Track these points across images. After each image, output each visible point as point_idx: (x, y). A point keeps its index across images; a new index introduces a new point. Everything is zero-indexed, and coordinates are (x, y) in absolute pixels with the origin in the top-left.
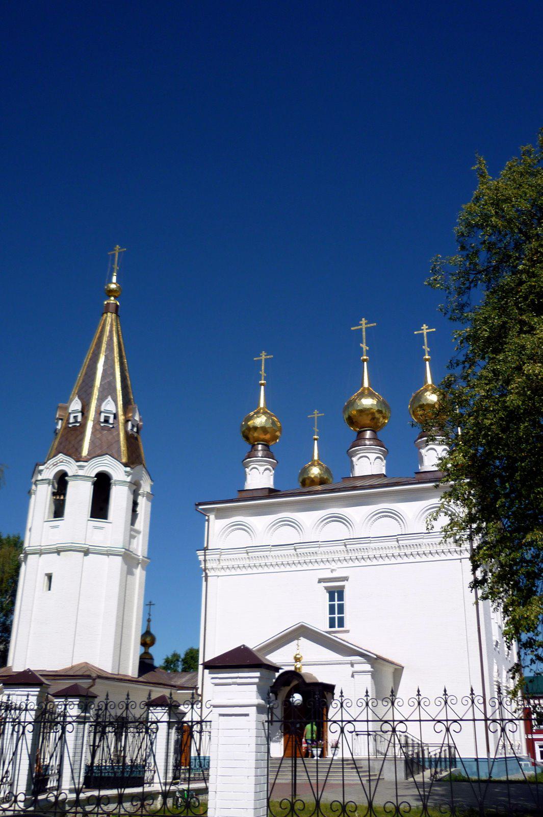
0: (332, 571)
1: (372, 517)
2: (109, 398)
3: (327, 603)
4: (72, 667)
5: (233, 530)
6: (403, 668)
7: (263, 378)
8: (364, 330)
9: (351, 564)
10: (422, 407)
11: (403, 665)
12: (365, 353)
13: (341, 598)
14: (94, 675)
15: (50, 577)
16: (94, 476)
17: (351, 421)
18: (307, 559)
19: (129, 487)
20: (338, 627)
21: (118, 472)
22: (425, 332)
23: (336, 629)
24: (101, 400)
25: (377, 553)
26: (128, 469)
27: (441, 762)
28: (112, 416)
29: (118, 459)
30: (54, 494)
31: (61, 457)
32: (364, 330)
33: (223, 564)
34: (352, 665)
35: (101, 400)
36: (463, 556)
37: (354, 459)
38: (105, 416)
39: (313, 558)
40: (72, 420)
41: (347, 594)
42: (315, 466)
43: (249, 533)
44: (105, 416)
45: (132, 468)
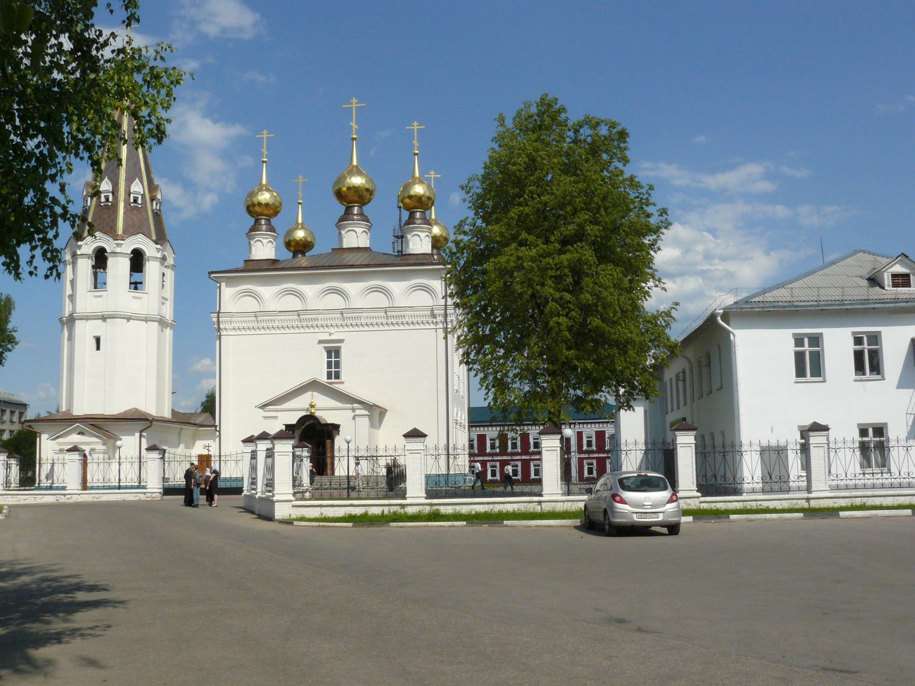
0: (330, 334)
1: (365, 291)
2: (137, 180)
3: (325, 360)
4: (126, 412)
5: (242, 297)
6: (387, 410)
7: (265, 156)
8: (354, 109)
9: (346, 329)
10: (410, 197)
11: (387, 408)
12: (354, 132)
14: (150, 419)
15: (98, 340)
16: (130, 253)
17: (339, 195)
18: (310, 324)
21: (150, 249)
22: (416, 128)
23: (333, 380)
24: (129, 181)
25: (369, 321)
26: (159, 246)
28: (140, 197)
29: (149, 237)
30: (93, 267)
32: (354, 109)
33: (236, 325)
34: (354, 410)
35: (129, 181)
36: (438, 327)
37: (343, 232)
38: (134, 197)
39: (314, 323)
40: (103, 199)
42: (301, 229)
43: (259, 303)
44: (134, 197)
45: (161, 245)
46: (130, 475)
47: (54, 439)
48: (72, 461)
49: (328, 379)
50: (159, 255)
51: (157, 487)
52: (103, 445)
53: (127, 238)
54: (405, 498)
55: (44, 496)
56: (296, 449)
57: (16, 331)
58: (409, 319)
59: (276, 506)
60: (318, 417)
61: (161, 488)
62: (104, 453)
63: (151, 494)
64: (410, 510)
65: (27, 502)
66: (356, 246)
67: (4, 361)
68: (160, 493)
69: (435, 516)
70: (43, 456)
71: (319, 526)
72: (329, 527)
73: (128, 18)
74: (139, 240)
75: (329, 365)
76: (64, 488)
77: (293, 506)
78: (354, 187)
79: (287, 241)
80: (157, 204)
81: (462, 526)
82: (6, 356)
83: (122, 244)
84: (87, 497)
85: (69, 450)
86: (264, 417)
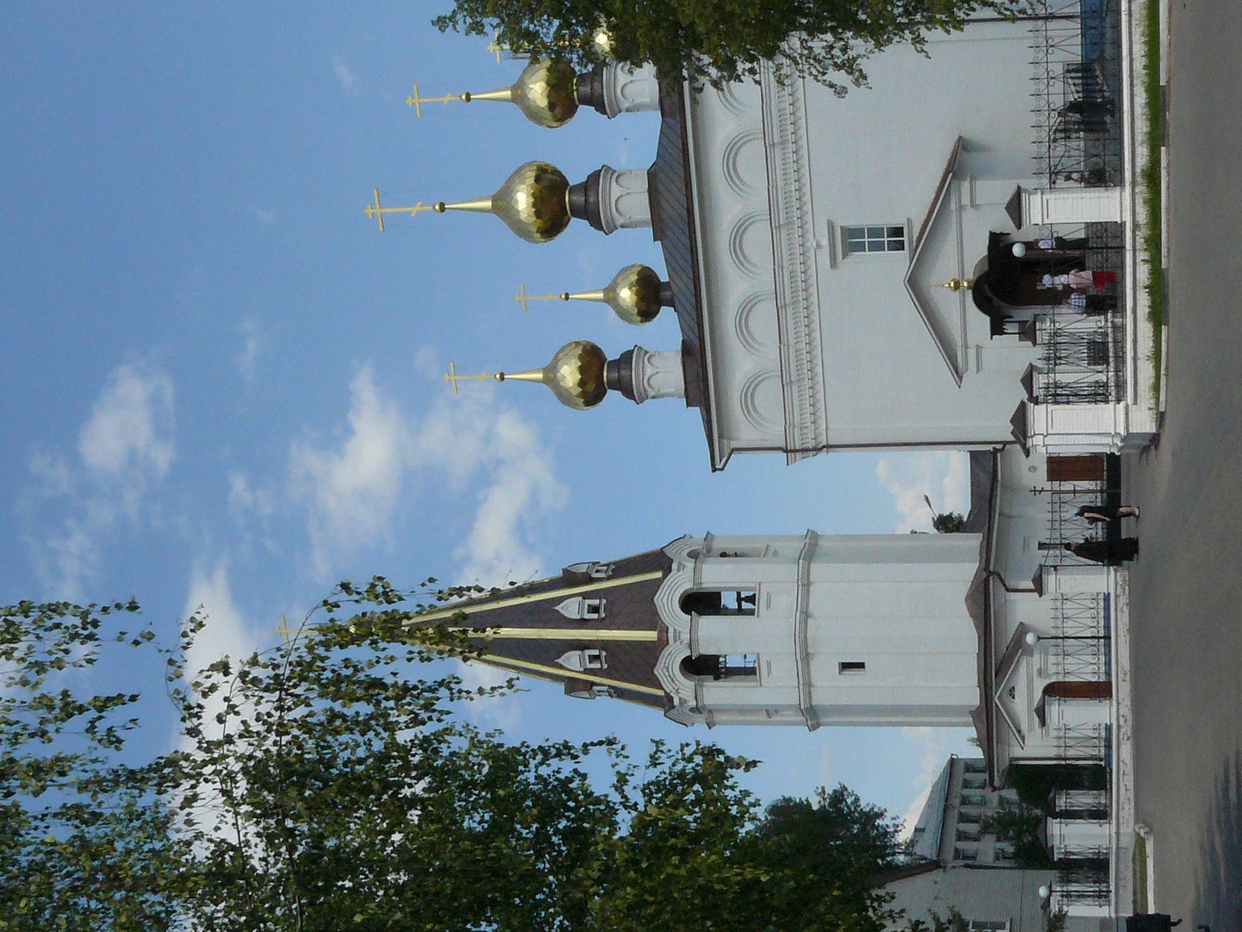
0: (819, 246)
2: (558, 608)
4: (972, 615)
5: (755, 409)
9: (808, 218)
13: (858, 232)
14: (984, 575)
15: (846, 666)
19: (702, 563)
20: (903, 236)
21: (680, 582)
22: (416, 101)
23: (905, 239)
26: (674, 566)
27: (1087, 84)
29: (657, 584)
30: (717, 678)
31: (660, 671)
33: (808, 419)
38: (588, 613)
40: (596, 665)
41: (852, 222)
46: (1084, 602)
47: (1023, 739)
48: (1061, 715)
49: (903, 249)
50: (690, 564)
51: (1106, 576)
52: (1032, 656)
53: (662, 622)
54: (1123, 224)
55: (1121, 759)
56: (1039, 341)
57: (823, 788)
58: (785, 101)
59: (1135, 432)
60: (977, 276)
61: (1108, 569)
62: (1046, 654)
63: (1119, 587)
64: (1142, 217)
65: (1131, 787)
66: (647, 194)
67: (876, 810)
68: (1116, 571)
69: (1152, 176)
70: (1052, 752)
71: (1166, 375)
72: (1168, 347)
73: (626, 809)
74: (665, 600)
75: (877, 247)
76: (1108, 728)
77: (1135, 403)
78: (534, 205)
79: (639, 318)
80: (597, 571)
81: (1168, 154)
82: (868, 805)
83: (675, 630)
84: (1122, 689)
85: (1043, 723)
86: (978, 371)
